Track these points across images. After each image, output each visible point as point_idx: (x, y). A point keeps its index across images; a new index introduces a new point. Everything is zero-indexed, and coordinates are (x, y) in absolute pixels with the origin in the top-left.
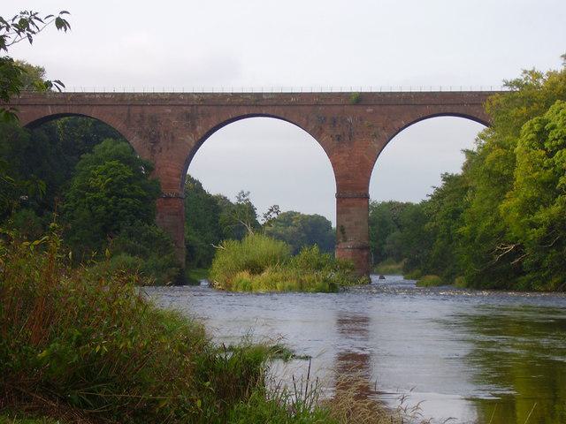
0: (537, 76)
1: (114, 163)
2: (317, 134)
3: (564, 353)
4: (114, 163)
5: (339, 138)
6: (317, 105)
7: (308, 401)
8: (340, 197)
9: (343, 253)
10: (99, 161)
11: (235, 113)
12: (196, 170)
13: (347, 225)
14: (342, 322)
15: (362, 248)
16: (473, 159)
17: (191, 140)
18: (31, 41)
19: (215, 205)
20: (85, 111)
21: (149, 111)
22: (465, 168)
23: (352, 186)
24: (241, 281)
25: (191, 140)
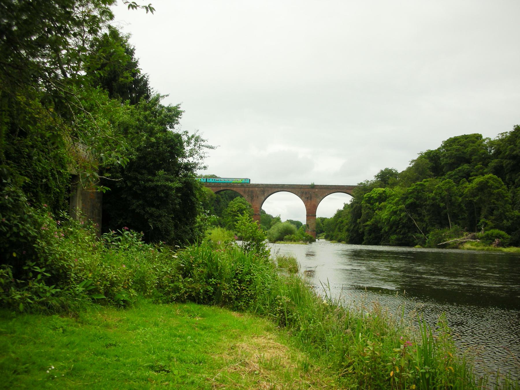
0: (368, 181)
1: (240, 204)
2: (301, 197)
3: (519, 276)
4: (240, 204)
5: (307, 198)
6: (301, 188)
7: (514, 378)
8: (308, 216)
9: (309, 234)
10: (236, 203)
11: (276, 190)
12: (263, 208)
13: (309, 224)
14: (307, 255)
15: (314, 231)
16: (346, 206)
17: (263, 198)
18: (211, 148)
19: (269, 217)
20: (232, 189)
21: (251, 189)
22: (344, 208)
23: (311, 212)
24: (107, 326)
25: (263, 198)
